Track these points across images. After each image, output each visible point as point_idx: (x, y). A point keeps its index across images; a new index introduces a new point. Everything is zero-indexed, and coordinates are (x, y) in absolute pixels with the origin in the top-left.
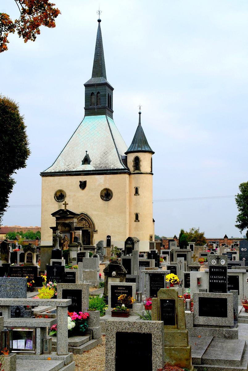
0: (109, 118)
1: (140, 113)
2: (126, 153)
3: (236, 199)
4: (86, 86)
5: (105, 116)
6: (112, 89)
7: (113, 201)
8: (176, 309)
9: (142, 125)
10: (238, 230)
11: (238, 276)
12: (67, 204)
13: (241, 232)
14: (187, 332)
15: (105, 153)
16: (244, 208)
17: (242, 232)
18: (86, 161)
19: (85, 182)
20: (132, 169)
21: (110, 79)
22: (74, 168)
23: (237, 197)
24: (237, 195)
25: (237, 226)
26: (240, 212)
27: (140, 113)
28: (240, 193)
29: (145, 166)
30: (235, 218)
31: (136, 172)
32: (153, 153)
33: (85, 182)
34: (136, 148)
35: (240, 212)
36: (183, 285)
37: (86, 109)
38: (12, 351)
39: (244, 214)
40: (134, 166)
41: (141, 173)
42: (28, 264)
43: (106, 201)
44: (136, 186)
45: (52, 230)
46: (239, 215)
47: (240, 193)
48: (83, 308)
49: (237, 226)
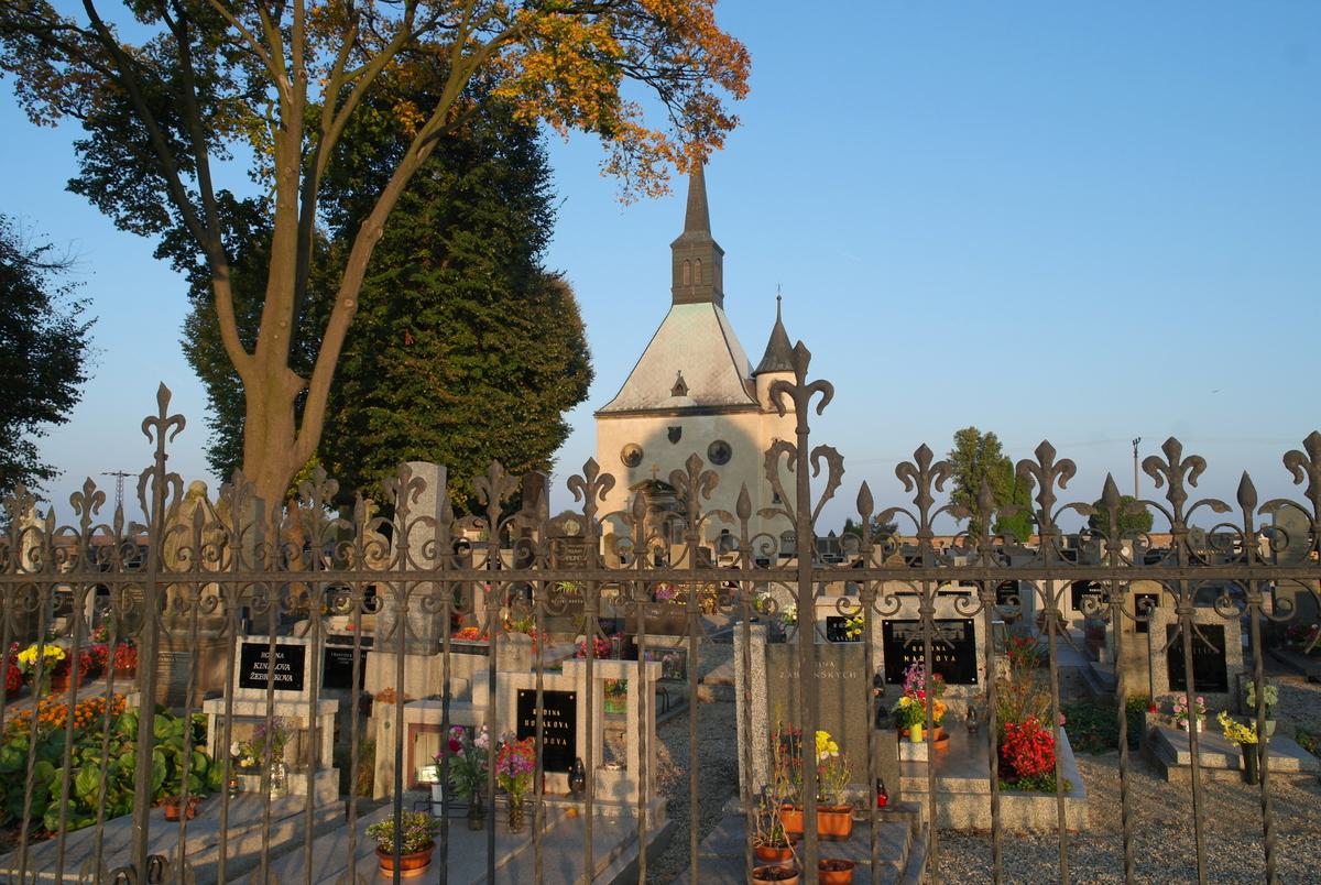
0: (717, 307)
1: (779, 299)
4: (674, 246)
5: (711, 304)
6: (722, 253)
8: (147, 705)
11: (520, 691)
15: (715, 375)
16: (963, 477)
17: (960, 523)
18: (680, 389)
19: (679, 430)
20: (766, 403)
21: (718, 234)
22: (657, 403)
27: (779, 299)
28: (956, 449)
33: (679, 430)
37: (676, 288)
42: (506, 699)
46: (955, 491)
47: (956, 449)
48: (247, 690)
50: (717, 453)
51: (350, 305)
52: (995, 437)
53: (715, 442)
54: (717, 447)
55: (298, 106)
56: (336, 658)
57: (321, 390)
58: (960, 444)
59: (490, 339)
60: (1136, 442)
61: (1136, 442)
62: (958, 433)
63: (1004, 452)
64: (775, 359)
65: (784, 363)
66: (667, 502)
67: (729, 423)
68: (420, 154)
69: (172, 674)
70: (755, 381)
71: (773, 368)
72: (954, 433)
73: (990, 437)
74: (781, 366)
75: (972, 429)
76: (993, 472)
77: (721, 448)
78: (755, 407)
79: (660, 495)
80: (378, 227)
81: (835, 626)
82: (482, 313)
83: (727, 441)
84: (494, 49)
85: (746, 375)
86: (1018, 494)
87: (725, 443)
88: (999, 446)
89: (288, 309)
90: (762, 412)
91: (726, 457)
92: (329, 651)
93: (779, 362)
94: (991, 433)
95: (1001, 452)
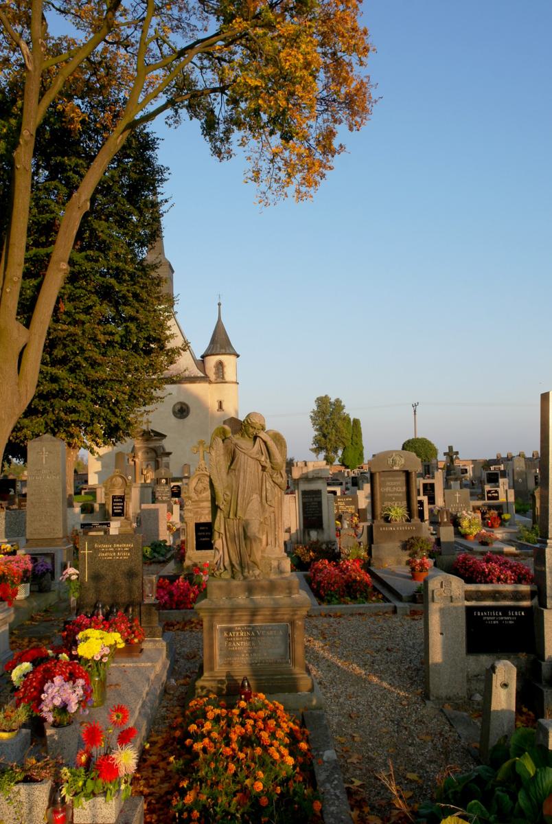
1: (219, 304)
2: (203, 357)
3: (311, 417)
7: (190, 419)
9: (223, 320)
10: (314, 455)
12: (151, 422)
13: (317, 456)
14: (207, 773)
20: (212, 377)
23: (312, 414)
24: (312, 410)
25: (312, 450)
26: (316, 433)
27: (219, 304)
29: (229, 374)
30: (311, 440)
31: (219, 380)
32: (238, 356)
34: (218, 350)
35: (316, 433)
36: (129, 783)
38: (201, 528)
39: (139, 762)
40: (215, 374)
41: (226, 382)
43: (181, 418)
44: (220, 399)
45: (96, 475)
49: (312, 450)
50: (179, 411)
51: (64, 267)
52: (341, 402)
53: (178, 403)
54: (178, 407)
55: (37, 73)
56: (481, 617)
57: (39, 344)
58: (319, 406)
59: (127, 311)
60: (415, 406)
61: (415, 406)
62: (318, 399)
63: (346, 411)
64: (218, 345)
65: (225, 349)
66: (158, 445)
67: (186, 391)
68: (118, 141)
69: (252, 652)
70: (203, 361)
71: (217, 352)
72: (315, 399)
73: (338, 401)
74: (223, 351)
75: (326, 396)
76: (339, 424)
77: (182, 408)
78: (205, 379)
79: (152, 440)
80: (87, 200)
81: (381, 529)
82: (121, 289)
83: (187, 403)
84: (89, 79)
85: (199, 358)
86: (354, 438)
87: (184, 404)
88: (343, 408)
89: (19, 265)
90: (210, 382)
91: (185, 414)
92: (469, 610)
93: (221, 348)
94: (338, 399)
95: (344, 411)
